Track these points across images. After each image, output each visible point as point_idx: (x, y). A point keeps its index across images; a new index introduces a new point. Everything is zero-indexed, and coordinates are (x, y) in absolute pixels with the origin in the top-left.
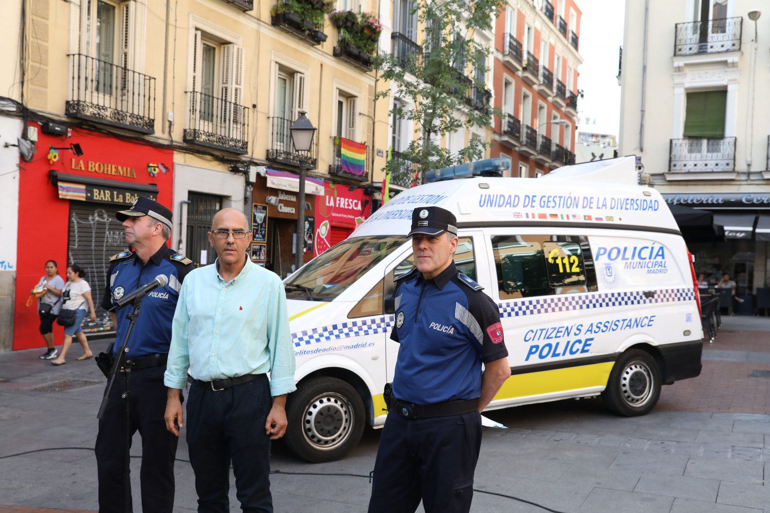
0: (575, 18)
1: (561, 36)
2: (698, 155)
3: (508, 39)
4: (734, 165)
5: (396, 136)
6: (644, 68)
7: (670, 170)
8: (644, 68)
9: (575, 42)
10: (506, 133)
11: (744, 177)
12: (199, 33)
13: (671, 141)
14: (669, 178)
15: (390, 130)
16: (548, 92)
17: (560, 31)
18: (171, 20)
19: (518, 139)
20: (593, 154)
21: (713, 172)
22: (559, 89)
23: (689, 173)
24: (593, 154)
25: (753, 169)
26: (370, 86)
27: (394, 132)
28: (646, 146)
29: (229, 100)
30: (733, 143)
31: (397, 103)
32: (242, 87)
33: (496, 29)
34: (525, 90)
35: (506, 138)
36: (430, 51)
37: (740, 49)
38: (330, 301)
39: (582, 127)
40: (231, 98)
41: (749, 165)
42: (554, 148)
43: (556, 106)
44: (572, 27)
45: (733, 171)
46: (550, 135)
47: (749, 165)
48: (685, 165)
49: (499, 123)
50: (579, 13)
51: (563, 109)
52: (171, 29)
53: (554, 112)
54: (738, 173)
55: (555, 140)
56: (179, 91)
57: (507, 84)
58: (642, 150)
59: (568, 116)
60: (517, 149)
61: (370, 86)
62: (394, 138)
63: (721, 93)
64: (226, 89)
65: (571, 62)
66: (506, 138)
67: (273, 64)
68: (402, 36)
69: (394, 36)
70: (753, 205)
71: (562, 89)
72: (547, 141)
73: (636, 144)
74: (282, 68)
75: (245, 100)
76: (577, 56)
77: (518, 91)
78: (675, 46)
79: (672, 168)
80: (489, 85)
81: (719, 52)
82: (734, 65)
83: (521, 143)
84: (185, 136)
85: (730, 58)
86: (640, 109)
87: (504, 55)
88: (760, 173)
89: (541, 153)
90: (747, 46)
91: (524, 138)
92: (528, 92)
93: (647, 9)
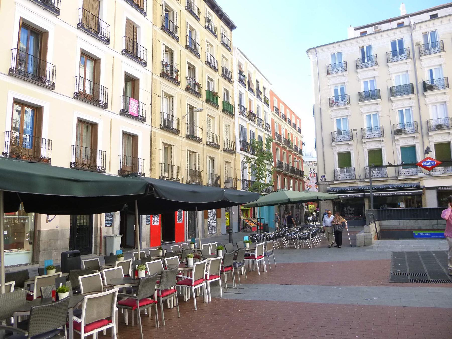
0: (299, 122)
1: (294, 130)
2: (343, 174)
3: (276, 134)
4: (355, 177)
5: (243, 173)
6: (323, 146)
7: (335, 179)
8: (323, 146)
9: (300, 131)
10: (278, 167)
11: (358, 181)
12: (188, 151)
13: (334, 170)
14: (335, 182)
15: (241, 172)
16: (292, 150)
17: (294, 128)
18: (182, 149)
19: (282, 168)
20: (310, 169)
21: (349, 180)
22: (295, 148)
23: (341, 180)
24: (310, 169)
25: (361, 178)
26: (234, 158)
27: (242, 172)
28: (326, 172)
29: (196, 170)
30: (354, 170)
31: (242, 162)
32: (200, 165)
33: (272, 132)
34: (283, 151)
35: (278, 169)
36: (306, 236)
37: (352, 140)
38: (62, 253)
39: (305, 159)
40: (197, 169)
41: (360, 177)
42: (295, 170)
43: (295, 155)
44: (298, 125)
45: (355, 179)
46: (294, 166)
47: (360, 177)
48: (340, 178)
49: (275, 164)
50: (300, 120)
51: (298, 155)
52: (182, 151)
53: (295, 157)
54: (357, 179)
55: (296, 167)
56: (184, 169)
57: (277, 149)
58: (325, 173)
59: (300, 158)
60: (282, 172)
61: (234, 158)
62: (242, 174)
63: (349, 154)
64: (195, 166)
65: (299, 138)
66: (278, 169)
67: (207, 156)
68: (243, 141)
69: (240, 141)
70: (362, 190)
71: (296, 148)
72: (293, 168)
73: (323, 171)
74: (210, 157)
75: (201, 170)
76: (301, 135)
77: (281, 152)
78: (332, 139)
79: (336, 179)
80: (271, 151)
81: (346, 141)
82: (351, 144)
83: (284, 170)
84: (186, 182)
85: (350, 142)
86: (323, 160)
87: (276, 140)
88: (363, 179)
89: (291, 172)
90: (354, 138)
91: (284, 168)
92: (285, 151)
93: (322, 127)
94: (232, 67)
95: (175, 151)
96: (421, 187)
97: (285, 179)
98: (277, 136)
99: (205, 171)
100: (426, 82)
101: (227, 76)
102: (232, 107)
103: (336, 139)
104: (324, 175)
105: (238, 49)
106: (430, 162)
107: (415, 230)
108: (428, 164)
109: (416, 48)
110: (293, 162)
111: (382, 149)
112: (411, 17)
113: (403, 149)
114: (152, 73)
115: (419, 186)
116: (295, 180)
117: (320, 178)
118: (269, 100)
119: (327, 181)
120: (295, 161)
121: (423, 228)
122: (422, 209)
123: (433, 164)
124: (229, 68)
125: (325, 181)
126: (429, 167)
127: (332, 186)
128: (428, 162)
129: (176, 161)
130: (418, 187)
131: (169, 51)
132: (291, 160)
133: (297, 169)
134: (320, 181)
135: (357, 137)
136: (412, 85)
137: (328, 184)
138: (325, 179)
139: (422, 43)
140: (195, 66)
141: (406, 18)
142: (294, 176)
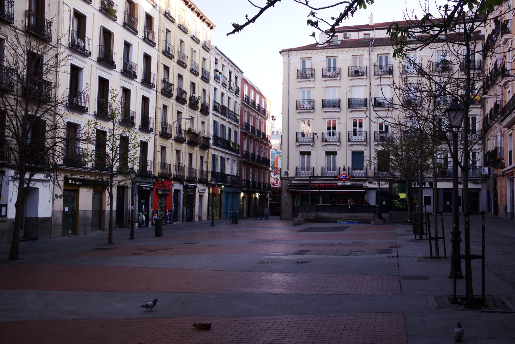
3: (244, 124)
32: (183, 162)
40: (181, 165)
41: (318, 175)
42: (262, 159)
58: (288, 169)
72: (259, 157)
73: (287, 168)
94: (210, 69)
95: (168, 151)
96: (365, 188)
97: (250, 169)
98: (245, 126)
99: (186, 166)
100: (376, 98)
101: (205, 79)
102: (208, 108)
103: (300, 139)
104: (287, 171)
105: (216, 48)
106: (345, 176)
107: (338, 219)
108: (343, 177)
109: (372, 67)
110: (259, 151)
111: (337, 152)
112: (376, 31)
113: (354, 153)
114: (157, 92)
115: (363, 187)
116: (256, 142)
117: (283, 173)
118: (240, 89)
119: (289, 177)
120: (262, 150)
121: (343, 218)
122: (319, 205)
123: (346, 177)
124: (207, 69)
125: (288, 177)
126: (344, 179)
127: (293, 182)
128: (344, 176)
129: (168, 161)
130: (361, 187)
131: (166, 68)
132: (257, 149)
133: (263, 158)
134: (283, 176)
135: (318, 139)
136: (366, 99)
137: (289, 179)
138: (288, 175)
139: (378, 63)
140: (182, 75)
141: (372, 31)
142: (259, 165)
